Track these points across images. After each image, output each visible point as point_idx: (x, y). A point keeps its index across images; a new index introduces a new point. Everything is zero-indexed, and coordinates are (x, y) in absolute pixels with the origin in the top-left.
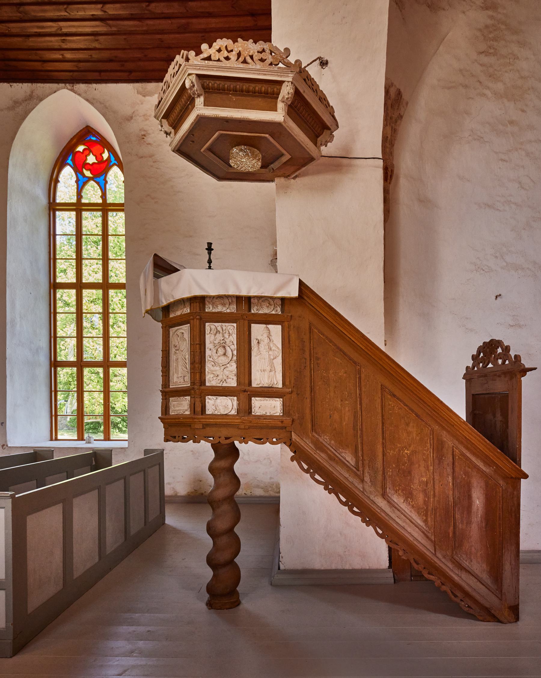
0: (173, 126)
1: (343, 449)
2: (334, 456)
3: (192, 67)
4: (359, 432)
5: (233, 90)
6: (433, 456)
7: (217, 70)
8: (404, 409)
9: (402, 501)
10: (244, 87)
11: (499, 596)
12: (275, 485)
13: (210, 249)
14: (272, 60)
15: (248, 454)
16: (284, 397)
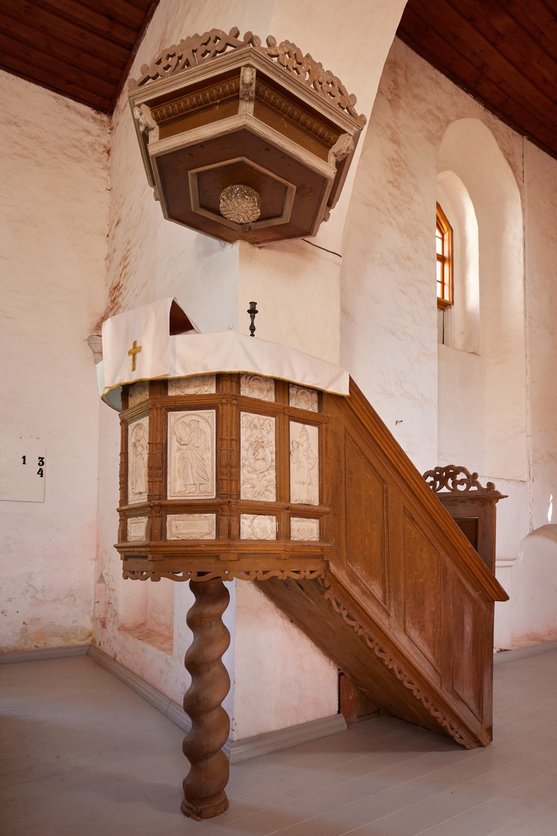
0: (161, 121)
1: (372, 580)
2: (366, 589)
3: (256, 58)
4: (386, 560)
5: (289, 114)
6: (440, 584)
7: (282, 79)
8: (419, 534)
9: (418, 634)
10: (302, 118)
11: (481, 720)
12: (79, 630)
13: (253, 311)
14: (340, 101)
15: (43, 591)
16: (321, 519)
